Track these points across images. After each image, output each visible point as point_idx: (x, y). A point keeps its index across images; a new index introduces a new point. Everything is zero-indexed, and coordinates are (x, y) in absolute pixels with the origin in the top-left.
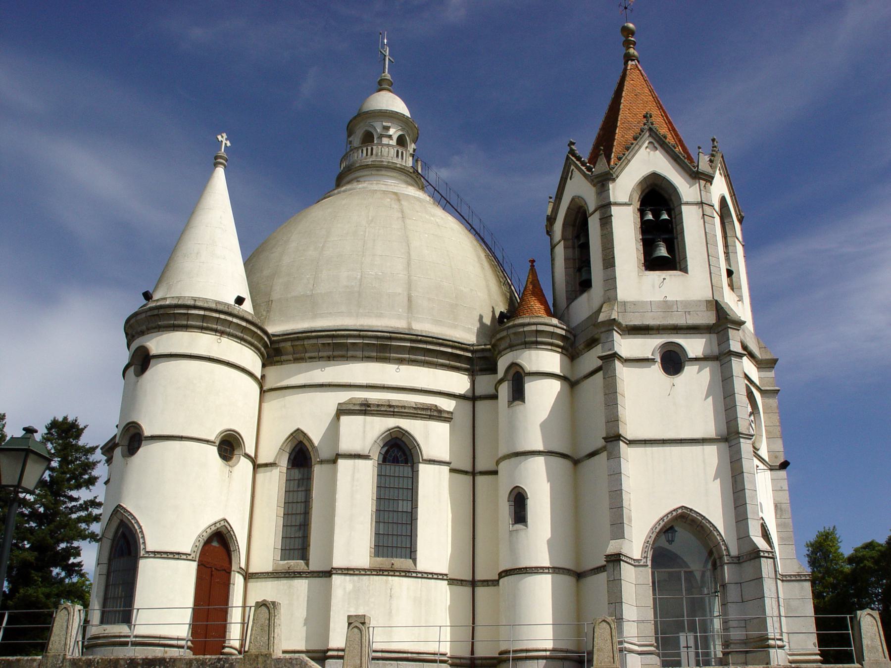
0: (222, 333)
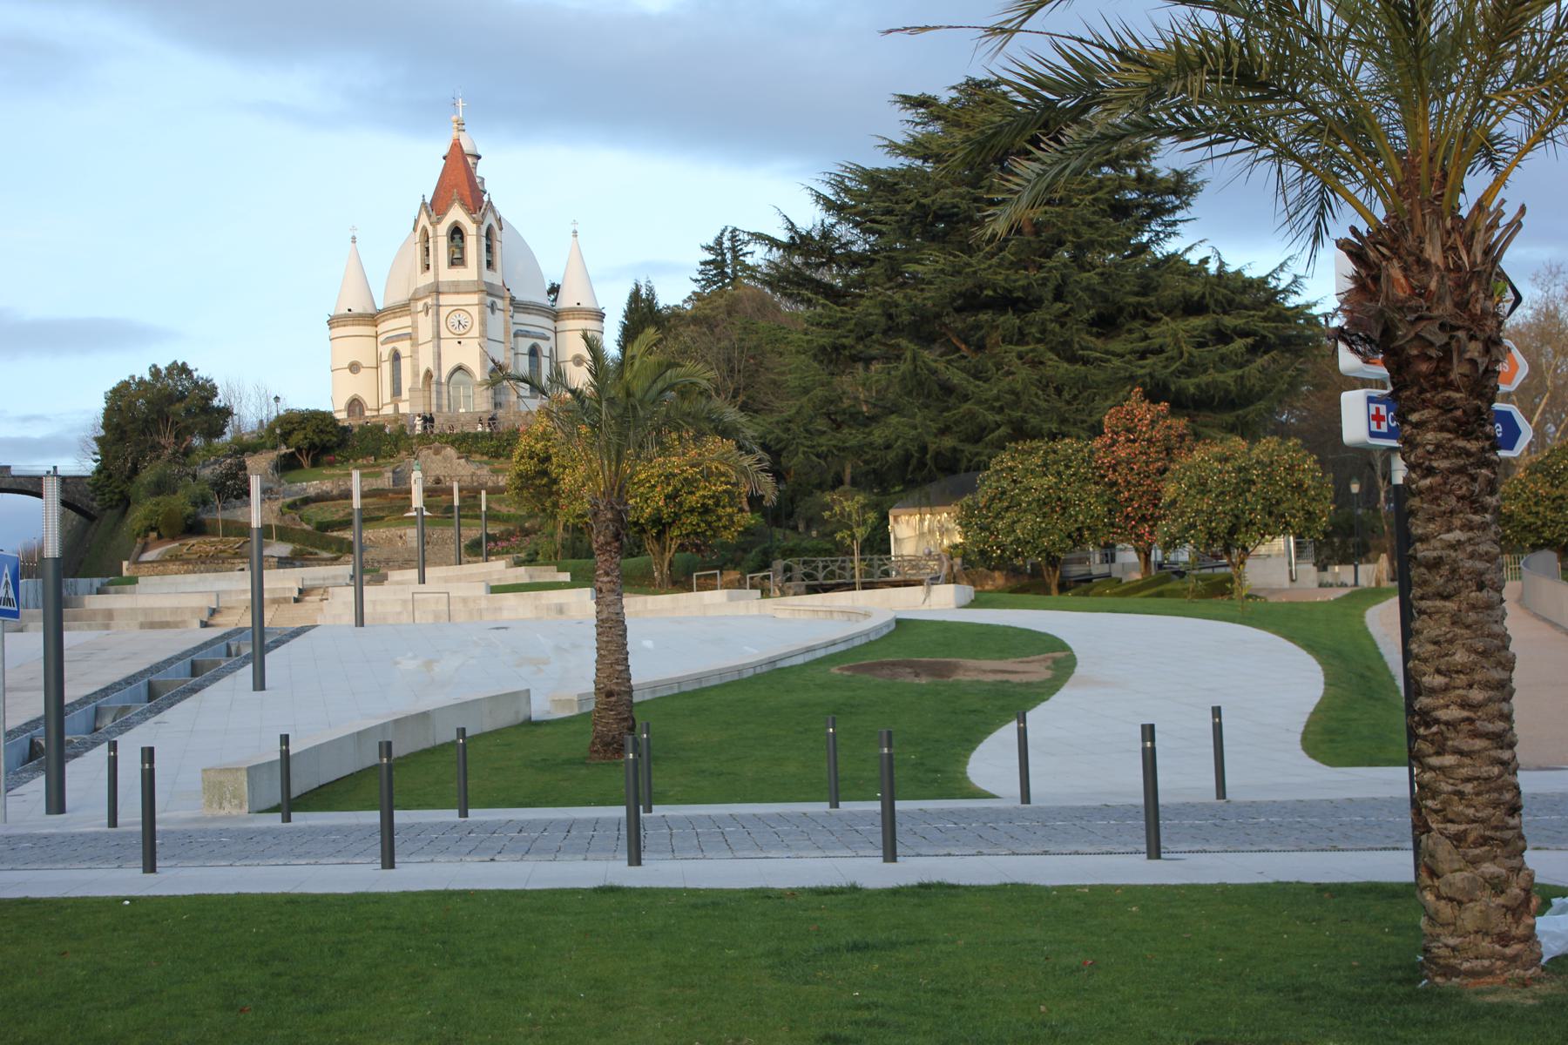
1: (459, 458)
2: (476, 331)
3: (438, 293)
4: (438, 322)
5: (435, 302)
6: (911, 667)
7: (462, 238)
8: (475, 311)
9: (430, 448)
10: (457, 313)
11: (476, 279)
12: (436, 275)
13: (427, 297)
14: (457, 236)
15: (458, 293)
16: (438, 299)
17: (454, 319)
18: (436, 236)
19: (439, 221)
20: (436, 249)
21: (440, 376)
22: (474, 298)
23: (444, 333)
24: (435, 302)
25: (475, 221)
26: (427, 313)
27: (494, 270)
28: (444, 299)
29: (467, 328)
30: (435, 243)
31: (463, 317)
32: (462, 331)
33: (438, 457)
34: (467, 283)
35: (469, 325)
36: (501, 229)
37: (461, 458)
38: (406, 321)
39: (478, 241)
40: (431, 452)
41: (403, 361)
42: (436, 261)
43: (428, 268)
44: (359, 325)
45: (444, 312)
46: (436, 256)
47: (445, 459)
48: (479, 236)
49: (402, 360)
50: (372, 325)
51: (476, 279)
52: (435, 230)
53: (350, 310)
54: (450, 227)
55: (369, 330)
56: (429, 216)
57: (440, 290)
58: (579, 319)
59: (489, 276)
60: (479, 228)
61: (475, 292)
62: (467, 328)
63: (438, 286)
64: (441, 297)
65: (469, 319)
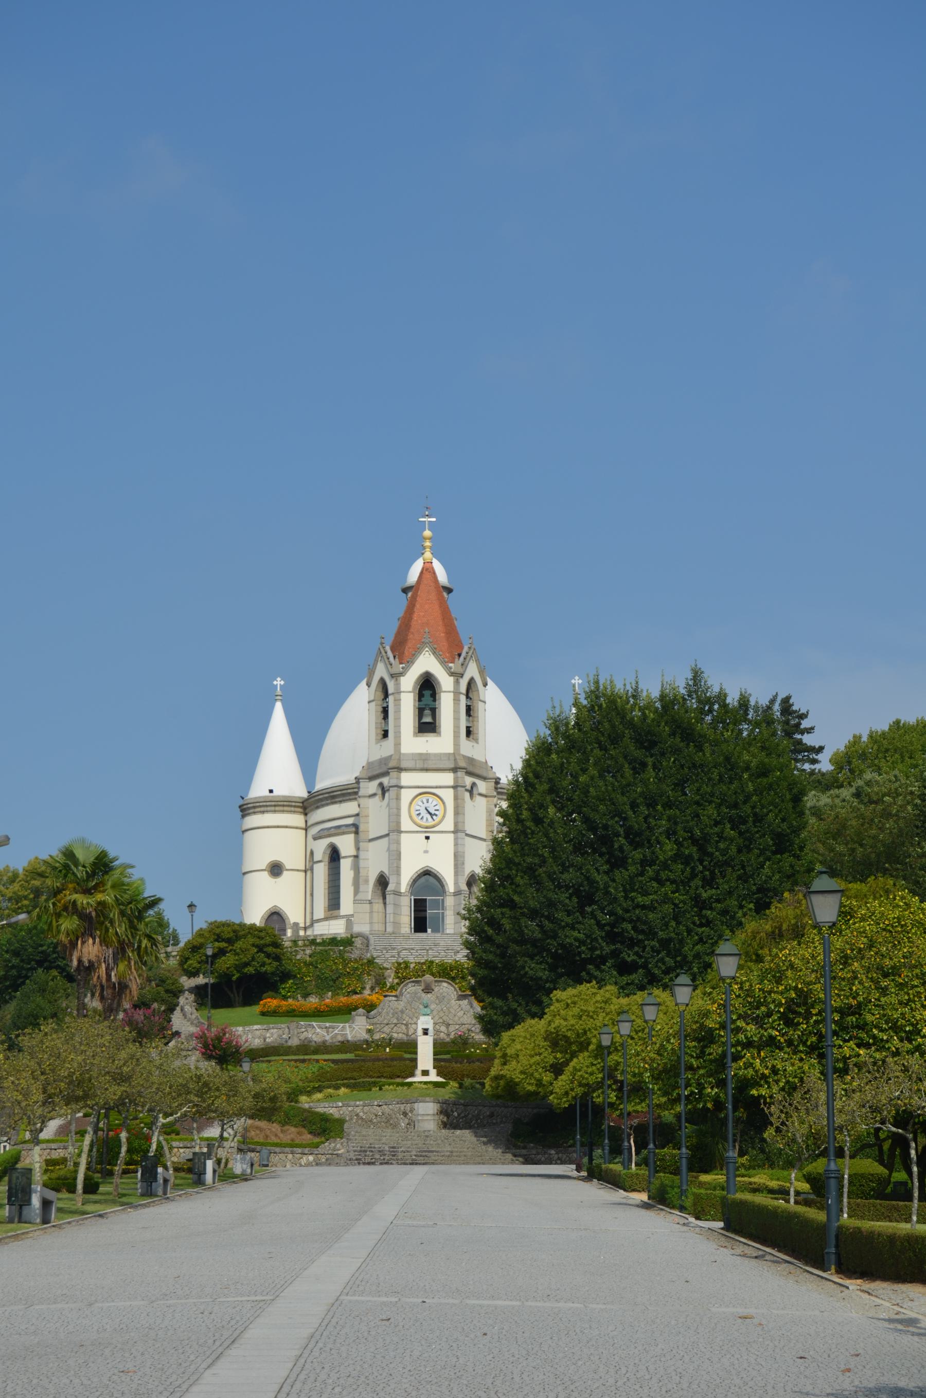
0: (263, 812)
1: (459, 999)
7: (434, 696)
10: (424, 798)
12: (398, 745)
14: (427, 693)
15: (427, 770)
18: (398, 692)
21: (398, 883)
22: (448, 778)
23: (406, 824)
28: (406, 778)
29: (437, 819)
30: (398, 701)
32: (431, 822)
33: (429, 995)
34: (439, 756)
35: (440, 814)
39: (456, 700)
42: (398, 726)
43: (385, 734)
47: (441, 999)
48: (456, 693)
49: (342, 861)
51: (451, 751)
52: (398, 685)
53: (271, 791)
54: (416, 683)
60: (457, 683)
65: (440, 806)
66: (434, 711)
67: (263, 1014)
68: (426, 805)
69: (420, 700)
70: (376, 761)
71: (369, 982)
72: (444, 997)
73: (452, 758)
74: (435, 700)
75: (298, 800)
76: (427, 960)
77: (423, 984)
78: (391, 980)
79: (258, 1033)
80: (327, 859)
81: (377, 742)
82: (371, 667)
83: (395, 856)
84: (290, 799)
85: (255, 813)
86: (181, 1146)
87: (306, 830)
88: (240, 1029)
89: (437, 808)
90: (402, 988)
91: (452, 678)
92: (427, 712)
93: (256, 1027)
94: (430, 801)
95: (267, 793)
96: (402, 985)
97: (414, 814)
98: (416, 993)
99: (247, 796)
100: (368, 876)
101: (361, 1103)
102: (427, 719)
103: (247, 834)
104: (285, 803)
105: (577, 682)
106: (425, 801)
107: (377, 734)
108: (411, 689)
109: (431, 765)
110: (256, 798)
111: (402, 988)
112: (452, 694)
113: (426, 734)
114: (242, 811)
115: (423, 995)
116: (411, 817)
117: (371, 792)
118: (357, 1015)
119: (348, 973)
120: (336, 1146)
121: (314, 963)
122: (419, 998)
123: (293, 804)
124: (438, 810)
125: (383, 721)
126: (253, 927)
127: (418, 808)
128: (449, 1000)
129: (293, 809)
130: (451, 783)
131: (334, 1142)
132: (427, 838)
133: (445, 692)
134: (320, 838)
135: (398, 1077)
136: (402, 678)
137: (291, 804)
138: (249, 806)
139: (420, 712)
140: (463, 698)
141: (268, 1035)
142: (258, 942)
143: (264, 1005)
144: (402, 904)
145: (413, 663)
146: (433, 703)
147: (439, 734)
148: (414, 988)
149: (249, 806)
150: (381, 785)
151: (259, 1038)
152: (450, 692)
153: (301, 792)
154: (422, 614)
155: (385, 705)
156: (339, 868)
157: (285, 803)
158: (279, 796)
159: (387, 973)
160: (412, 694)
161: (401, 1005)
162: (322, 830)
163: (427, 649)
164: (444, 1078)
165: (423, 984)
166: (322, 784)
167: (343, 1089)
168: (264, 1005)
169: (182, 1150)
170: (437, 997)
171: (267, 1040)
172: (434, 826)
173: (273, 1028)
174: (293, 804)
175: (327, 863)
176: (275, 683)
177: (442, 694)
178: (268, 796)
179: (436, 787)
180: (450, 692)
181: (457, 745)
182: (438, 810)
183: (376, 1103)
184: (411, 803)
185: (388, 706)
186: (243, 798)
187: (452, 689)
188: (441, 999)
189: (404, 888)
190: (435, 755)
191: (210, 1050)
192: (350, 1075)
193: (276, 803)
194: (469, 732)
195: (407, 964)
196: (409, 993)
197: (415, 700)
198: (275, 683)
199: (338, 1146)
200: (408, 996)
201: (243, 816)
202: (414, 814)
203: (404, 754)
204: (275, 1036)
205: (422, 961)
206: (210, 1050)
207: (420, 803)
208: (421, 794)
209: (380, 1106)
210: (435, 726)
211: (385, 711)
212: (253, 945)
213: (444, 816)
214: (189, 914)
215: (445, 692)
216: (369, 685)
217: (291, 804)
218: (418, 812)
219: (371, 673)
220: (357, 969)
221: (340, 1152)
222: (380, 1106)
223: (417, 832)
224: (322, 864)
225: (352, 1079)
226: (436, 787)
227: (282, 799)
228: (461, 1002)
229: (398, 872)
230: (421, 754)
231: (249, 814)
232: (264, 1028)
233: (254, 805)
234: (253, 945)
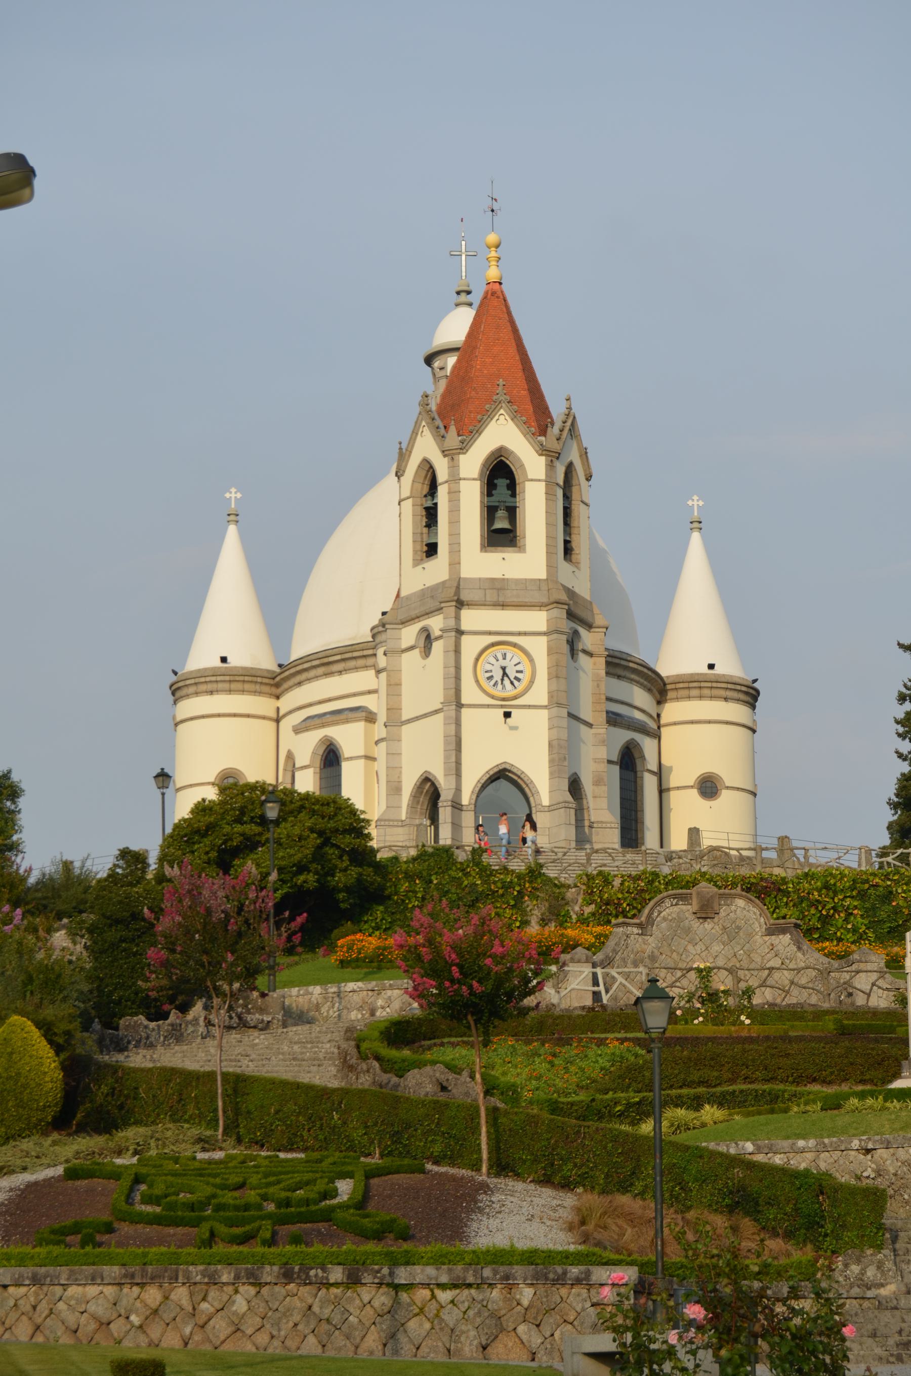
1: (770, 932)
2: (540, 693)
3: (460, 604)
4: (458, 668)
5: (452, 623)
6: (269, 1219)
7: (512, 487)
8: (539, 647)
9: (685, 898)
10: (499, 651)
11: (543, 575)
12: (455, 564)
13: (428, 614)
14: (502, 483)
15: (503, 606)
16: (458, 618)
17: (493, 666)
18: (455, 478)
19: (464, 448)
20: (455, 510)
21: (458, 790)
22: (538, 620)
23: (470, 693)
24: (452, 623)
25: (543, 451)
26: (427, 650)
27: (577, 565)
28: (470, 618)
29: (520, 686)
30: (454, 495)
31: (513, 658)
32: (510, 691)
33: (708, 925)
34: (524, 584)
35: (525, 677)
36: (589, 478)
37: (783, 931)
38: (363, 679)
39: (549, 494)
40: (687, 910)
41: (347, 768)
42: (455, 535)
43: (431, 550)
44: (243, 692)
45: (470, 646)
46: (455, 522)
47: (731, 933)
48: (550, 483)
49: (345, 765)
50: (271, 695)
51: (543, 575)
52: (454, 467)
53: (224, 660)
54: (484, 465)
55: (263, 705)
56: (440, 437)
57: (464, 596)
58: (712, 698)
59: (566, 573)
60: (550, 466)
61: (541, 606)
62: (520, 686)
63: (458, 588)
64: (465, 613)
65: (526, 666)
66: (512, 512)
67: (343, 964)
68: (503, 663)
69: (489, 494)
70: (415, 593)
71: (536, 910)
72: (739, 928)
73: (544, 587)
74: (514, 495)
75: (266, 675)
76: (644, 872)
77: (695, 901)
78: (577, 908)
79: (357, 998)
80: (318, 762)
81: (417, 562)
82: (404, 446)
83: (455, 745)
84: (253, 673)
85: (197, 694)
86: (444, 1279)
87: (278, 721)
88: (294, 991)
89: (519, 668)
90: (652, 909)
91: (543, 458)
92: (501, 513)
93: (351, 986)
94: (509, 656)
95: (218, 663)
96: (652, 903)
97: (482, 677)
98: (680, 919)
99: (184, 664)
100: (400, 782)
101: (812, 1143)
102: (501, 524)
103: (180, 727)
104: (246, 678)
105: (695, 503)
106: (500, 657)
107: (415, 552)
108: (476, 475)
109: (510, 597)
110: (199, 670)
111: (652, 909)
112: (544, 483)
113: (500, 548)
114: (173, 694)
115: (696, 924)
116: (477, 681)
117: (411, 642)
118: (572, 960)
119: (494, 892)
120: (863, 1272)
121: (425, 874)
122: (688, 931)
123: (259, 680)
124: (521, 672)
125: (425, 530)
126: (307, 797)
127: (489, 667)
128: (750, 936)
129: (258, 687)
130: (543, 628)
131: (858, 1261)
132: (507, 715)
133: (532, 480)
134: (307, 729)
135: (814, 1080)
136: (461, 456)
137: (255, 679)
138: (188, 682)
139: (490, 512)
140: (560, 493)
141: (380, 1002)
142: (321, 824)
143: (350, 948)
144: (463, 825)
145: (479, 432)
146: (512, 499)
147: (522, 549)
148: (676, 909)
149: (188, 682)
150: (426, 631)
151: (361, 1008)
152: (539, 480)
153: (267, 663)
154: (489, 360)
155: (429, 504)
156: (338, 776)
157: (246, 678)
158: (236, 667)
159: (571, 894)
160: (478, 483)
161: (652, 943)
162: (308, 718)
163: (502, 411)
164: (891, 1090)
165: (695, 901)
166: (298, 651)
167: (707, 1107)
168: (350, 948)
169: (444, 1296)
170: (724, 928)
171: (378, 1014)
172: (515, 698)
173: (391, 987)
174: (259, 680)
175: (318, 770)
176: (227, 495)
177: (528, 485)
178: (219, 668)
179: (520, 634)
180: (539, 480)
181: (551, 567)
182: (521, 672)
183: (855, 1144)
184: (477, 660)
185: (436, 504)
186: (175, 673)
187: (543, 477)
188: (731, 933)
189: (466, 798)
190: (517, 581)
191: (452, 981)
192: (695, 1076)
193: (232, 678)
194: (568, 550)
195: (607, 880)
196: (665, 919)
197: (482, 493)
198: (227, 495)
199: (871, 1272)
200: (664, 925)
201: (175, 702)
202: (482, 677)
203: (465, 579)
204: (396, 1005)
205: (634, 873)
206: (452, 981)
207: (493, 661)
208: (493, 645)
209: (868, 1151)
210: (515, 537)
211: (431, 514)
212: (312, 830)
213: (532, 682)
214: (158, 792)
215: (532, 480)
216: (399, 475)
217: (255, 679)
218: (489, 675)
219: (403, 456)
220: (511, 885)
221: (883, 1292)
222: (868, 1151)
223: (488, 706)
224: (311, 771)
225: (701, 1083)
226: (520, 634)
227: (241, 673)
228: (774, 939)
229: (456, 770)
230: (493, 580)
231: (182, 697)
232: (370, 986)
233: (197, 680)
234: (312, 830)
